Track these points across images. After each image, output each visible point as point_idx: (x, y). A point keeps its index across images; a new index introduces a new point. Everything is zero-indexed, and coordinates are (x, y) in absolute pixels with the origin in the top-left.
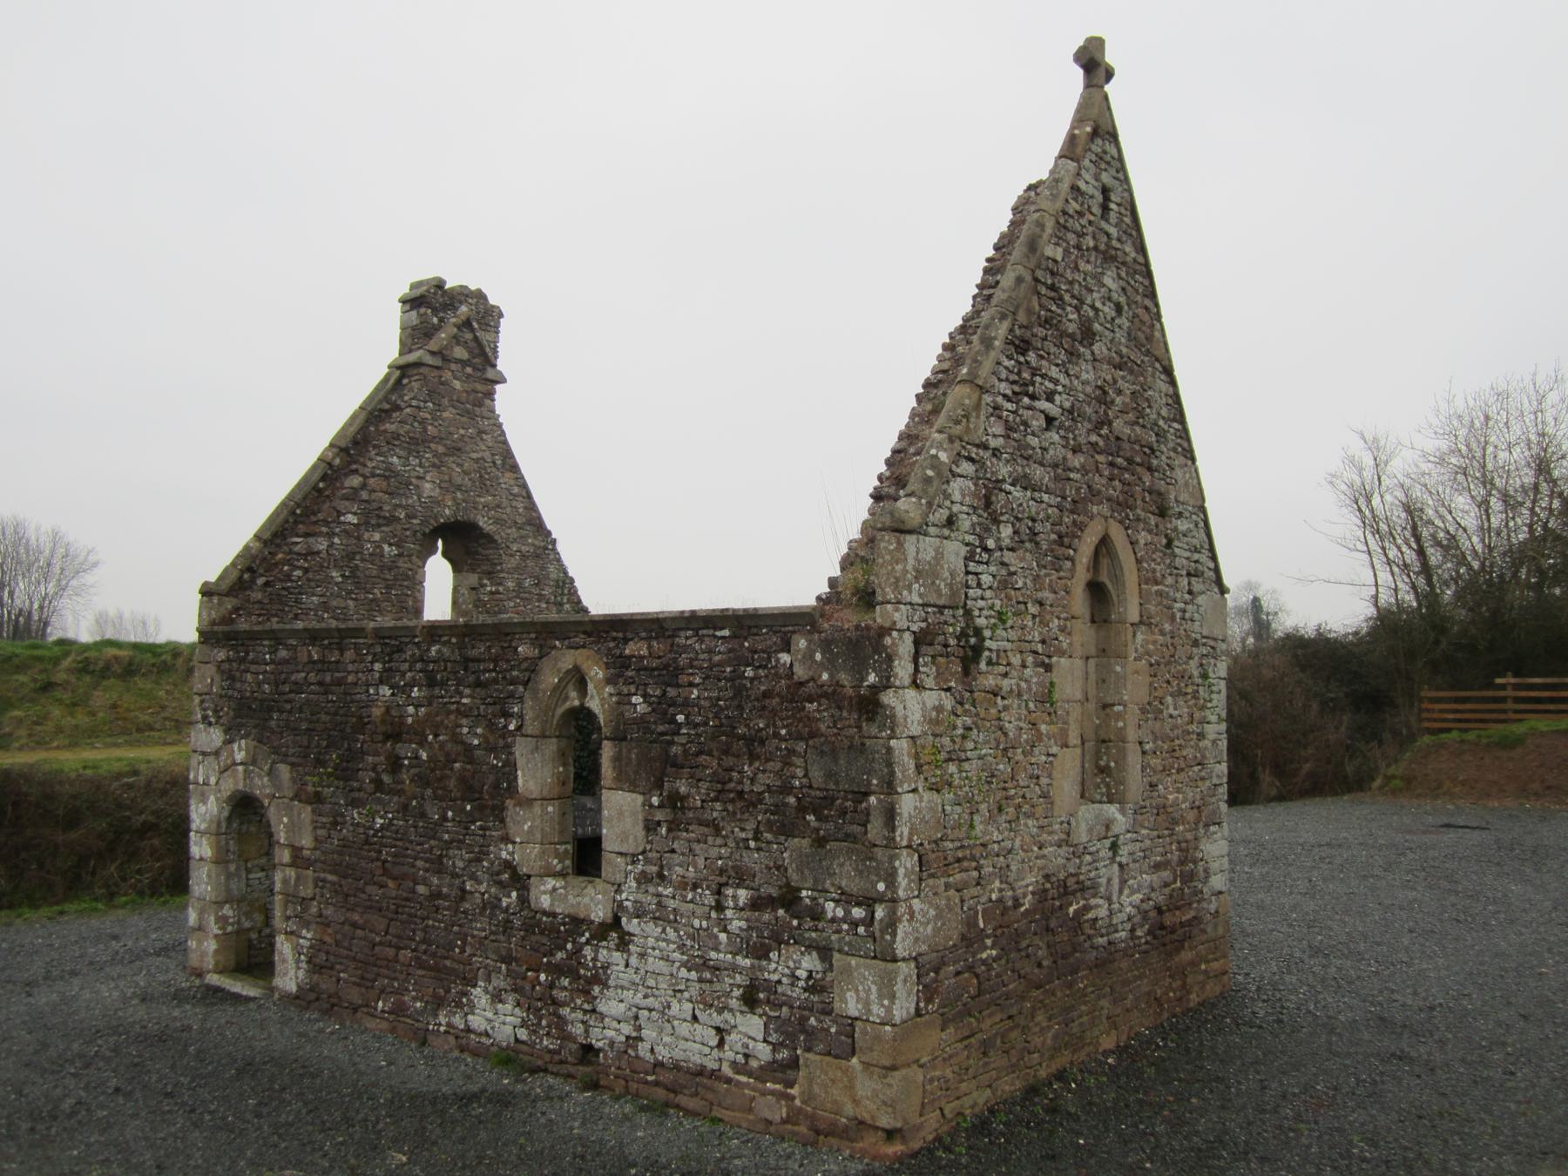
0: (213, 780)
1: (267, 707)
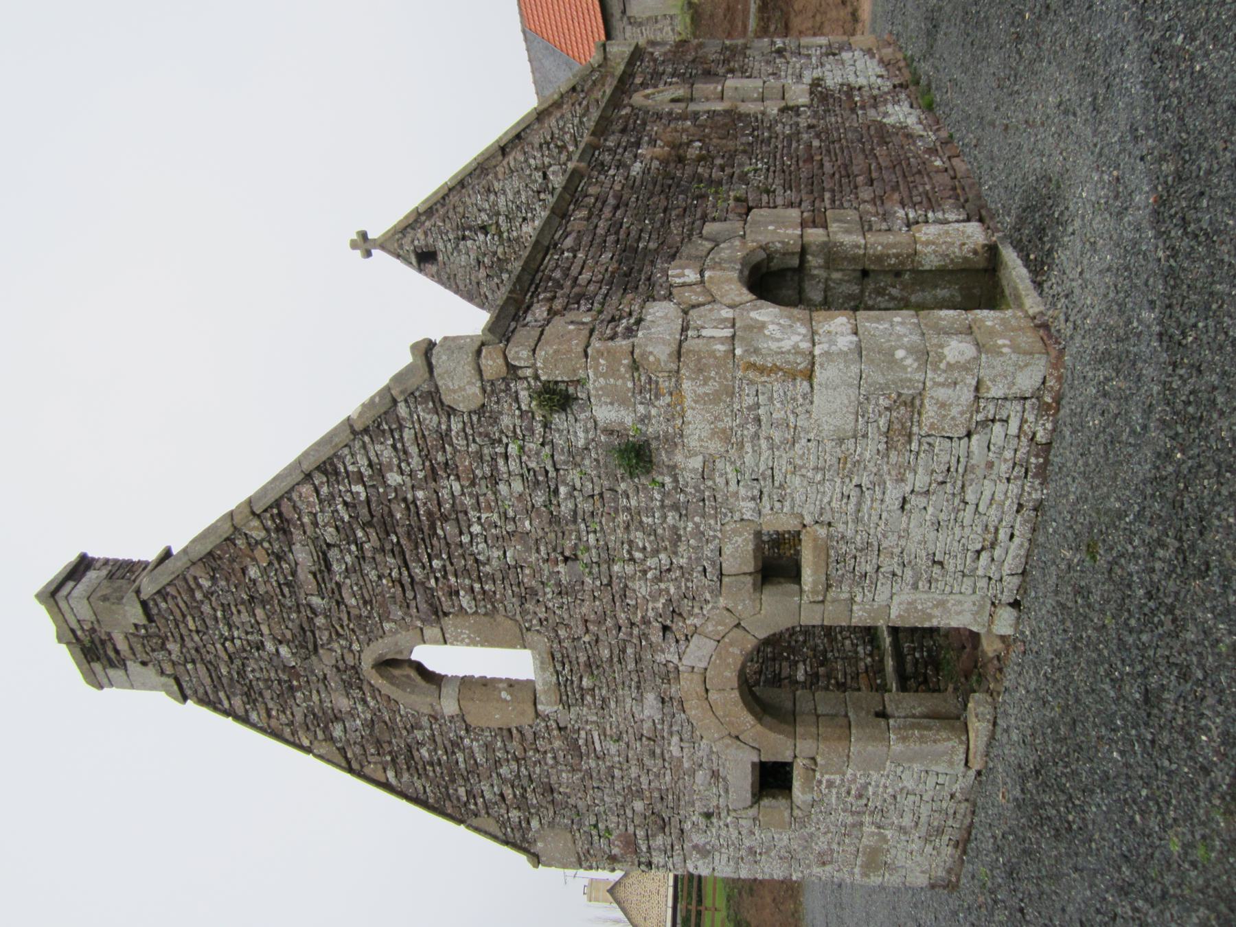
0: (727, 313)
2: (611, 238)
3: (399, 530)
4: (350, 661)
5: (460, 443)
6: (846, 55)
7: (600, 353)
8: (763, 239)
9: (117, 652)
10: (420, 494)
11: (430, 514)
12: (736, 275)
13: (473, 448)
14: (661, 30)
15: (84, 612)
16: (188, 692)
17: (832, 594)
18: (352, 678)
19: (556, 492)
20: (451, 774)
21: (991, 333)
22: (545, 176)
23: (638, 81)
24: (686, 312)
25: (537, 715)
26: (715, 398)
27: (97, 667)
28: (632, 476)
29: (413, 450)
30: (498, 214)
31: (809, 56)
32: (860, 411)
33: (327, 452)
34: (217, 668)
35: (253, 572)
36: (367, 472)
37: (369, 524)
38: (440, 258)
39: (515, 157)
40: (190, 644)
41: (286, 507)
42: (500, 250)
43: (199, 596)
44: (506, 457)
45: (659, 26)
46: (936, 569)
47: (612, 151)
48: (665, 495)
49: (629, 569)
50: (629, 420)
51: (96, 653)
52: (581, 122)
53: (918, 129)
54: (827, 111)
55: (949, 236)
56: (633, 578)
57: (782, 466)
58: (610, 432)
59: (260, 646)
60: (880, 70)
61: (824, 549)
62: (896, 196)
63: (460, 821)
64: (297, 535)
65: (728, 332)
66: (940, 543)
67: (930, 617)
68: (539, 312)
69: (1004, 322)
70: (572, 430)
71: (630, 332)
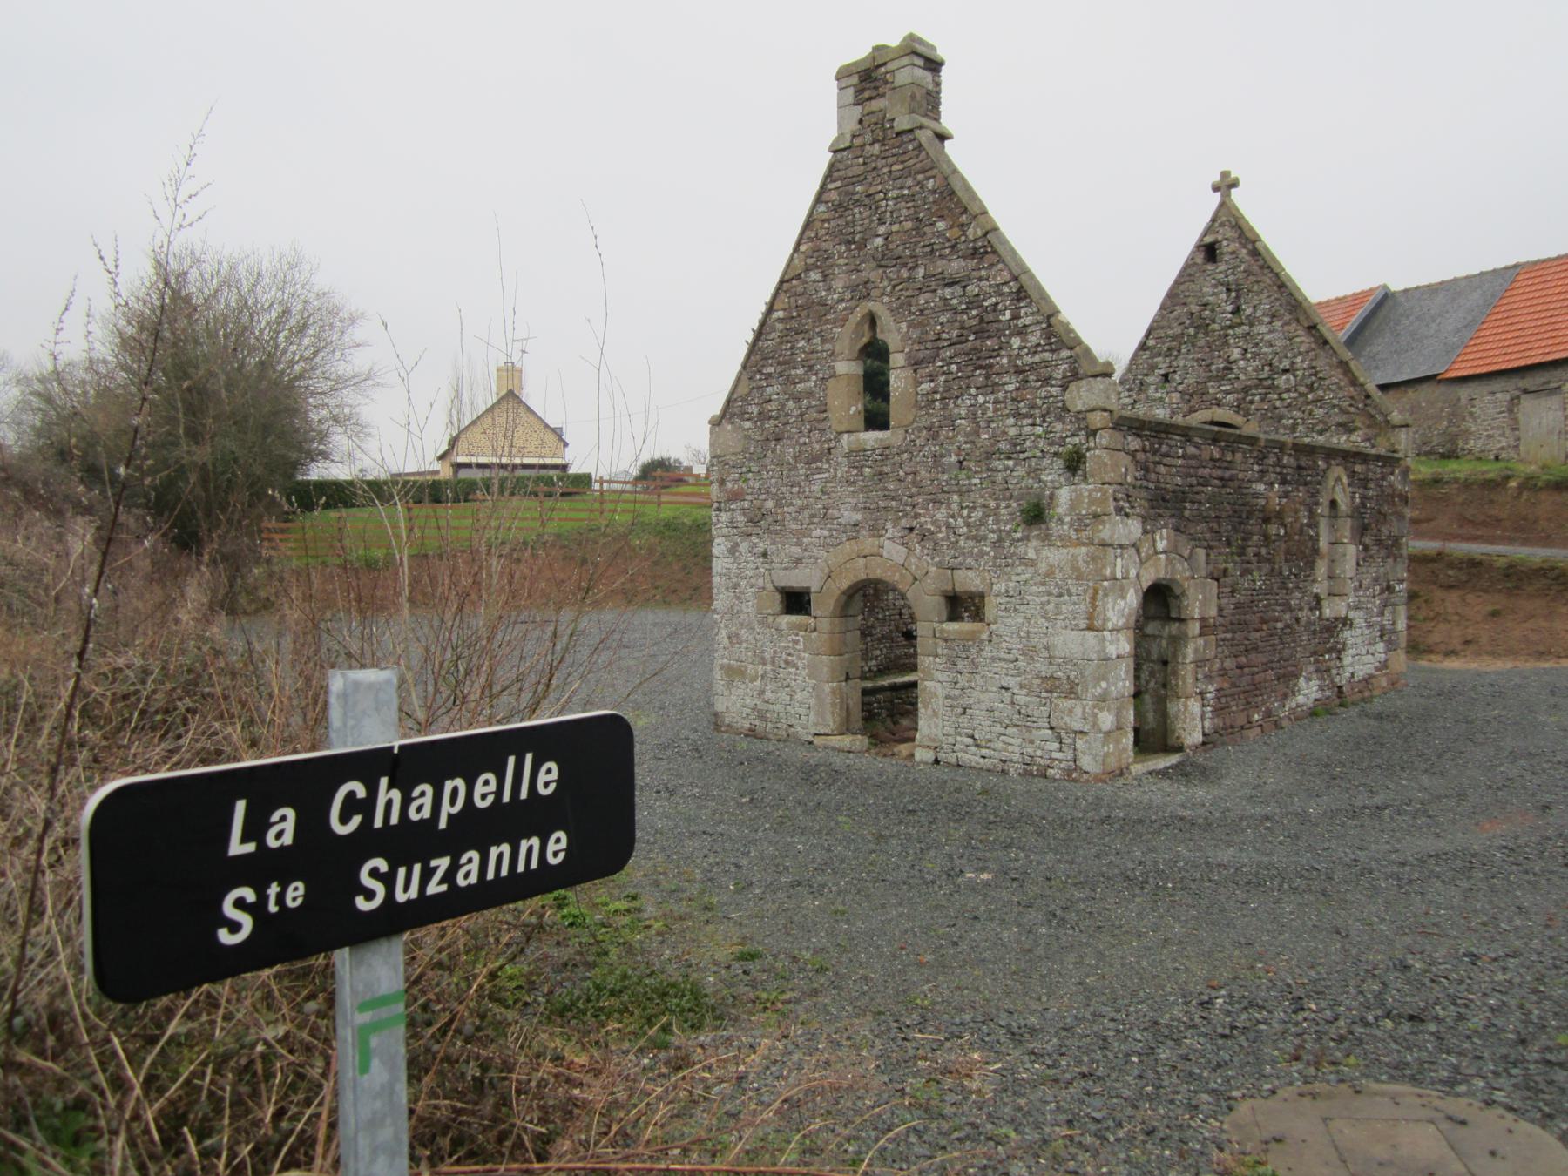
0: (1133, 573)
1: (1181, 496)
2: (1194, 481)
3: (978, 343)
4: (874, 293)
5: (1043, 392)
6: (1381, 647)
7: (1105, 493)
8: (1191, 592)
9: (870, 99)
10: (1005, 361)
11: (991, 366)
12: (1162, 575)
13: (1039, 402)
14: (1503, 435)
15: (902, 78)
16: (839, 156)
17: (941, 643)
18: (862, 291)
19: (1009, 458)
20: (784, 363)
21: (1117, 742)
22: (1286, 371)
23: (1358, 468)
24: (1134, 545)
25: (840, 433)
26: (1075, 568)
27: (855, 80)
28: (1022, 511)
29: (1037, 359)
30: (1251, 325)
31: (1382, 614)
32: (1067, 660)
33: (1034, 294)
34: (860, 182)
35: (941, 225)
36: (1021, 322)
37: (982, 320)
38: (1210, 267)
39: (1304, 340)
40: (880, 163)
41: (990, 258)
42: (1216, 326)
43: (920, 177)
44: (1033, 425)
45: (1508, 432)
46: (960, 710)
47: (1278, 463)
48: (1008, 533)
49: (955, 506)
50: (1060, 510)
51: (866, 79)
52: (1334, 406)
53: (1291, 704)
54: (1314, 632)
55: (1192, 720)
56: (949, 507)
57: (1029, 611)
58: (1052, 497)
59: (881, 222)
60: (1360, 675)
61: (973, 637)
62: (1226, 685)
63: (744, 367)
64: (972, 263)
65: (1119, 575)
66: (979, 713)
67: (926, 707)
68: (1134, 443)
69: (1125, 750)
70: (1052, 473)
71: (1119, 510)
